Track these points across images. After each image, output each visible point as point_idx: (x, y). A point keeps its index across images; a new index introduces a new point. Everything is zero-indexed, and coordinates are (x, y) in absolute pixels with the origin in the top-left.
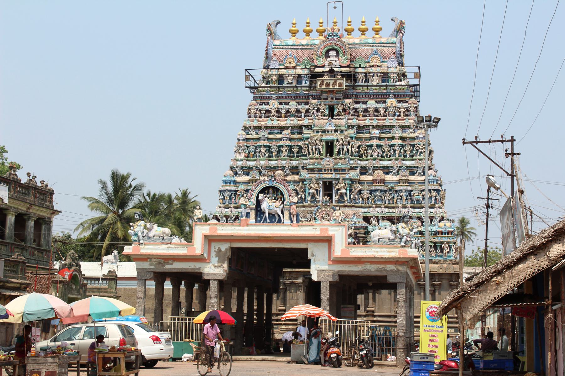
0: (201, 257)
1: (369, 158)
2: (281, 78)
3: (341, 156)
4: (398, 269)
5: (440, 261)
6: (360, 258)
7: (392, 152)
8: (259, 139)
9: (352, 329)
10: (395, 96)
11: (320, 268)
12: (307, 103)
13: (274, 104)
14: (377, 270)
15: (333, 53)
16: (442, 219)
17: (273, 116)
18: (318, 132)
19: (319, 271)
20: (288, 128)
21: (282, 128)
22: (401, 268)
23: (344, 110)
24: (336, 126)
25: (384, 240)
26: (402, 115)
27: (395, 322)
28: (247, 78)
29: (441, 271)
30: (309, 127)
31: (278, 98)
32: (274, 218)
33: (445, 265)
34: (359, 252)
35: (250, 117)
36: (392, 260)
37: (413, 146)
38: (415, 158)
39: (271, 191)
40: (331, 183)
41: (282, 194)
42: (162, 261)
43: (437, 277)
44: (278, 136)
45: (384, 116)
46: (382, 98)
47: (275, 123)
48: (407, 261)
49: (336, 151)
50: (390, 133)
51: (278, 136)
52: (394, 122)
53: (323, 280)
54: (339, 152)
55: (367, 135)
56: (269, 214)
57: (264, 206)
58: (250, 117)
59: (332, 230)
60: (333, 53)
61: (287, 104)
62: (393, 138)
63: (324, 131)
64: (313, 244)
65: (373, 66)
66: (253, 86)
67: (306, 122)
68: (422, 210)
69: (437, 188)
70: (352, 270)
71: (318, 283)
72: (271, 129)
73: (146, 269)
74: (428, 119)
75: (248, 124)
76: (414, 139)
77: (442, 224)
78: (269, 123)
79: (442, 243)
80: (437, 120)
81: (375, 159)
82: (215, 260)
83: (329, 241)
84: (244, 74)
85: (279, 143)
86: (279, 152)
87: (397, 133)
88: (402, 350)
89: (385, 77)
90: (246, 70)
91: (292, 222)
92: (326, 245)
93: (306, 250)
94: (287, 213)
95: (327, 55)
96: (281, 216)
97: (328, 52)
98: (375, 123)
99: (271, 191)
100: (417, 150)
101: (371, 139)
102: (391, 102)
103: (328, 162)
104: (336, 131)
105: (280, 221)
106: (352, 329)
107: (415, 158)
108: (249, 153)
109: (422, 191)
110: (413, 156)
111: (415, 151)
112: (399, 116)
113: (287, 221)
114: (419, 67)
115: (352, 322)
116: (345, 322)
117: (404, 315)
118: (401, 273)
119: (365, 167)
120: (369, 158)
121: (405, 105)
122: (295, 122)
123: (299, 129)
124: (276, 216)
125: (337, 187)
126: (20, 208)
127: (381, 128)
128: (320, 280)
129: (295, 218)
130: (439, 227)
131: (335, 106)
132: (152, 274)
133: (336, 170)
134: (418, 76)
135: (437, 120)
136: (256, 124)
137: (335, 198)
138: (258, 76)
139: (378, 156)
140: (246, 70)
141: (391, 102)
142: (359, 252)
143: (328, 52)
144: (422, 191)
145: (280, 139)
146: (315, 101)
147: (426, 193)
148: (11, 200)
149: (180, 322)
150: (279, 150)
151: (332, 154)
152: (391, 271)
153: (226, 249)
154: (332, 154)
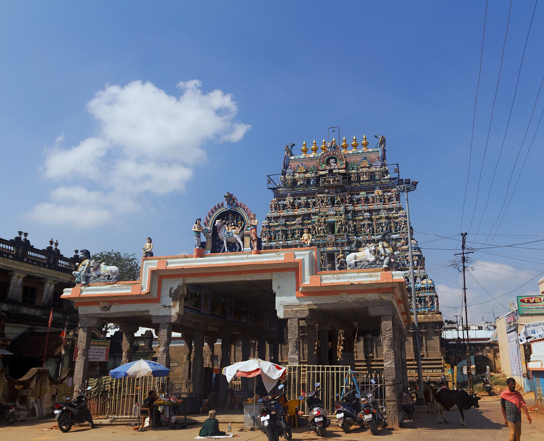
0: (149, 297)
1: (363, 234)
2: (295, 182)
3: (341, 234)
4: (381, 298)
5: (425, 312)
6: (334, 286)
7: (380, 228)
8: (278, 226)
9: (328, 378)
10: (380, 188)
11: (286, 302)
12: (314, 198)
13: (289, 200)
14: (356, 302)
15: (332, 161)
16: (425, 277)
17: (289, 208)
18: (322, 217)
19: (286, 306)
20: (300, 216)
21: (295, 217)
22: (385, 297)
23: (342, 200)
24: (335, 211)
25: (363, 263)
26: (387, 201)
27: (383, 365)
28: (269, 182)
29: (427, 320)
30: (315, 214)
31: (292, 195)
32: (233, 247)
33: (430, 315)
34: (330, 279)
35: (272, 210)
36: (374, 287)
37: (397, 223)
38: (399, 232)
39: (230, 216)
40: (333, 254)
41: (243, 219)
42: (107, 304)
43: (423, 326)
44: (293, 222)
45: (373, 202)
46: (370, 190)
47: (291, 213)
48: (393, 288)
49: (336, 230)
50: (378, 215)
51: (293, 222)
52: (381, 206)
53: (291, 316)
54: (339, 231)
55: (361, 218)
56: (228, 243)
57: (222, 235)
58: (272, 210)
59: (299, 255)
60: (332, 161)
61: (299, 199)
62: (381, 218)
63: (327, 216)
64: (278, 273)
65: (363, 167)
66: (272, 187)
67: (313, 210)
68: (407, 272)
69: (419, 253)
70: (326, 302)
71: (285, 321)
72: (288, 218)
73: (89, 314)
74: (408, 182)
75: (269, 215)
76: (397, 218)
77: (424, 281)
78: (284, 213)
79: (426, 297)
80: (415, 184)
81: (367, 235)
82: (167, 300)
83: (294, 268)
84: (266, 179)
85: (293, 228)
86: (293, 234)
87: (383, 214)
88: (392, 403)
89: (372, 175)
90: (268, 176)
91: (252, 248)
92: (293, 273)
93: (270, 282)
94: (247, 239)
95: (328, 163)
96: (241, 243)
97: (328, 160)
98: (366, 208)
99: (230, 216)
100: (401, 226)
101: (364, 219)
102: (378, 192)
103: (330, 237)
104: (336, 215)
105: (240, 250)
106: (328, 378)
107: (399, 232)
108: (271, 236)
109: (406, 257)
110: (397, 231)
111: (398, 227)
112: (385, 202)
113: (247, 249)
114: (398, 164)
115: (309, 369)
116: (323, 369)
117: (393, 357)
118: (386, 303)
119: (360, 241)
120: (363, 234)
121: (389, 194)
122: (305, 211)
123: (308, 216)
124: (237, 245)
125: (338, 257)
126: (61, 278)
127: (370, 211)
128: (287, 316)
129: (255, 243)
130: (422, 284)
131: (335, 198)
132: (96, 320)
133: (337, 245)
134: (397, 171)
135: (415, 184)
136: (276, 214)
137: (337, 266)
138: (278, 180)
139: (370, 232)
140: (268, 176)
141: (378, 192)
142: (330, 279)
143: (328, 160)
144: (406, 257)
145: (294, 225)
146: (321, 195)
147: (409, 258)
148: (187, 311)
149: (321, 372)
150: (294, 232)
151: (333, 232)
152: (374, 301)
153: (179, 287)
154: (333, 232)
